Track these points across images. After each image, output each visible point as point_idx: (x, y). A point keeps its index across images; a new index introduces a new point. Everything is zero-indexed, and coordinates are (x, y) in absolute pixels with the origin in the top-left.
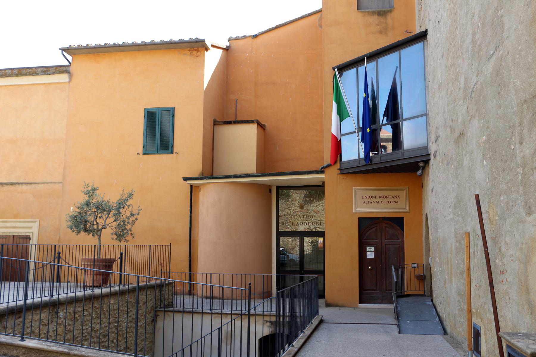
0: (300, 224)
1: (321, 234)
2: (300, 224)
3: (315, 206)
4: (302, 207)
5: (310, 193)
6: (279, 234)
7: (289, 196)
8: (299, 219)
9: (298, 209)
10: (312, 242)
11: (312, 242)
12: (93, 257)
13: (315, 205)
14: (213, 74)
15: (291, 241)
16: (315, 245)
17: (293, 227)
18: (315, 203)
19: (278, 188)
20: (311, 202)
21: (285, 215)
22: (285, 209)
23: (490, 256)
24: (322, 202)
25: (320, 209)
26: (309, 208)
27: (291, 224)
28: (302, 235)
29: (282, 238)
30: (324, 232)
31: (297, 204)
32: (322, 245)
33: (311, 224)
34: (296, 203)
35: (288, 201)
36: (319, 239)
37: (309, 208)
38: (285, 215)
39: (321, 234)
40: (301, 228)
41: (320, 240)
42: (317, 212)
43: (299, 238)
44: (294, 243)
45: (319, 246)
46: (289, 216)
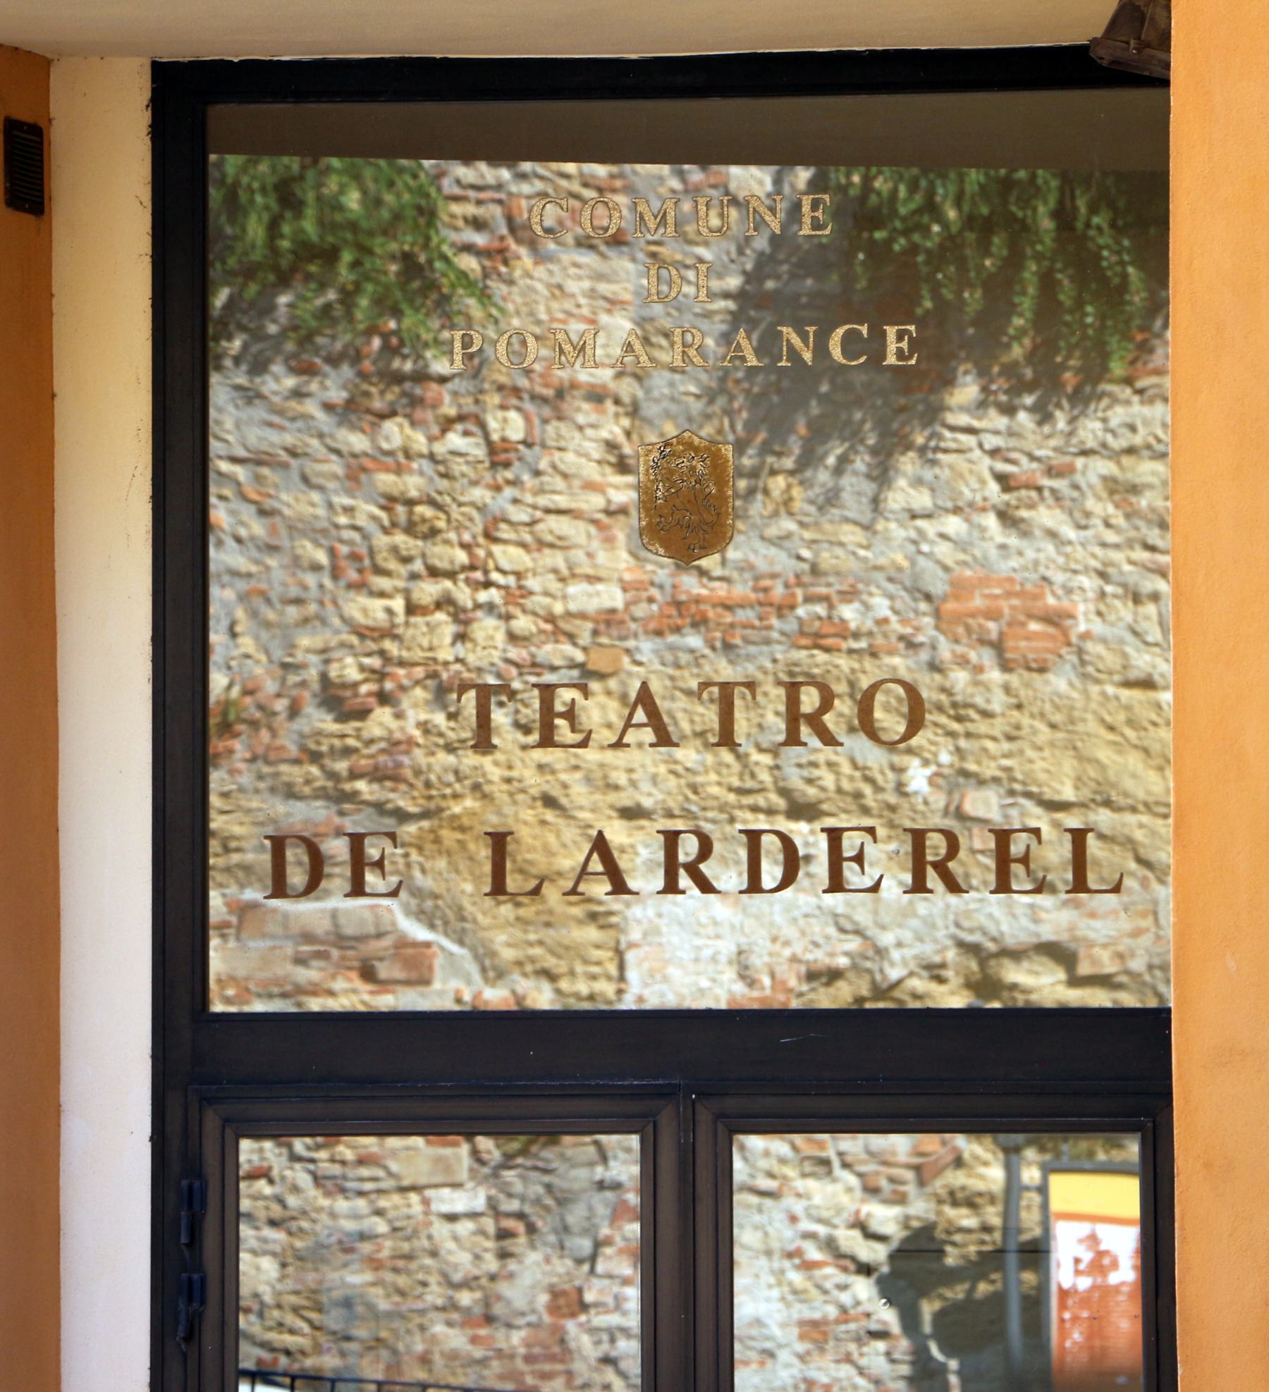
0: (644, 874)
1: (1094, 1073)
2: (644, 874)
3: (959, 513)
4: (686, 515)
5: (861, 216)
6: (229, 1078)
7: (422, 283)
8: (645, 771)
9: (611, 571)
10: (913, 1266)
11: (913, 1266)
12: (951, 418)
13: (974, 474)
14: (153, 479)
15: (462, 1249)
16: (964, 1328)
17: (501, 928)
18: (978, 429)
19: (194, 102)
20: (899, 413)
21: (335, 698)
22: (358, 569)
23: (212, 610)
24: (1124, 414)
25: (1065, 553)
26: (846, 546)
27: (468, 888)
28: (703, 1083)
29: (273, 1171)
30: (1154, 1023)
31: (588, 466)
32: (1126, 1327)
33: (885, 861)
34: (584, 442)
35: (410, 391)
36: (1069, 1191)
37: (846, 546)
38: (335, 698)
39: (1094, 1073)
40: (692, 953)
41: (1089, 1216)
42: (1024, 634)
43: (634, 1141)
44: (533, 1274)
45: (1068, 1338)
46: (417, 709)
